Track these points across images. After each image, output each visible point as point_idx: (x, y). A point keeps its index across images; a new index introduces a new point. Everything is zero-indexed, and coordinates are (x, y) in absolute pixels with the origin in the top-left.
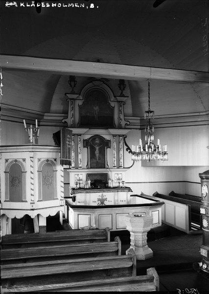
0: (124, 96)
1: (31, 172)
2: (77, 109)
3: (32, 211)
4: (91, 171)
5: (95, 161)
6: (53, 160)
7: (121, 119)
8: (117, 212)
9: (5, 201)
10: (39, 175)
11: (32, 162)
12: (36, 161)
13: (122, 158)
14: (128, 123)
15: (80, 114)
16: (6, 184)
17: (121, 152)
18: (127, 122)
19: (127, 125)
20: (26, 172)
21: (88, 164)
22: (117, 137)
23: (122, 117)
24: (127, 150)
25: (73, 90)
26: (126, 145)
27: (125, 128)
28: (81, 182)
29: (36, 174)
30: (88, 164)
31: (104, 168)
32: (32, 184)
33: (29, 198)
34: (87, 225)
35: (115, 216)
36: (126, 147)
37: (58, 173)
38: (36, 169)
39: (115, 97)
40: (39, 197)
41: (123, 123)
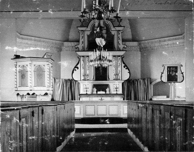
0: (121, 26)
1: (30, 71)
2: (86, 37)
3: (31, 91)
4: (96, 83)
5: (191, 90)
6: (35, 67)
7: (119, 44)
8: (98, 104)
9: (19, 87)
10: (35, 73)
11: (30, 66)
12: (33, 66)
13: (120, 73)
14: (126, 47)
15: (88, 41)
16: (19, 78)
17: (119, 69)
18: (124, 46)
19: (125, 48)
20: (28, 71)
21: (94, 77)
22: (116, 57)
23: (120, 42)
24: (124, 67)
25: (82, 24)
26: (124, 63)
27: (123, 51)
28: (88, 90)
29: (33, 72)
30: (94, 77)
31: (106, 80)
32: (31, 78)
33: (29, 84)
34: (58, 100)
35: (97, 107)
36: (123, 65)
37: (45, 72)
38: (33, 70)
39: (114, 27)
40: (35, 84)
41: (121, 46)
